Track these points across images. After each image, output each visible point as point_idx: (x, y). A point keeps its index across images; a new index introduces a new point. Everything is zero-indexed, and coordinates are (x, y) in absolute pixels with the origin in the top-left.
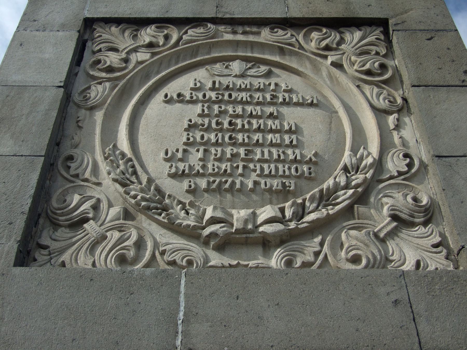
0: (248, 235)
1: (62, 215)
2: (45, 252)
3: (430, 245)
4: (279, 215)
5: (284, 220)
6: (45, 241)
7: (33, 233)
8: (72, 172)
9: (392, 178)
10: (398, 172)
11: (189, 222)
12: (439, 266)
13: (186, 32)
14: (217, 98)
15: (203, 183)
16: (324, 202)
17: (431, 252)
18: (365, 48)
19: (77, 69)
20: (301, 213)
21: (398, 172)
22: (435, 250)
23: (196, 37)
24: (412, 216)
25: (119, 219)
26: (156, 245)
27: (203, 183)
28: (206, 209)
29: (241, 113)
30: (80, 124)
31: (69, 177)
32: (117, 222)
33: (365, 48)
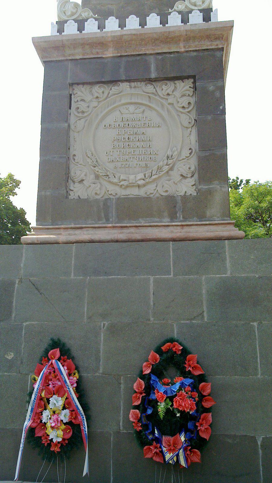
0: (133, 185)
1: (75, 178)
2: (73, 192)
3: (191, 185)
4: (143, 177)
5: (145, 178)
6: (72, 188)
7: (67, 185)
8: (76, 161)
9: (183, 159)
10: (186, 157)
11: (115, 181)
12: (192, 193)
13: (111, 89)
14: (124, 126)
15: (119, 164)
16: (159, 171)
17: (190, 188)
18: (184, 92)
19: (75, 379)
20: (150, 176)
21: (186, 157)
22: (192, 187)
23: (115, 92)
24: (187, 175)
25: (93, 179)
26: (106, 188)
27: (119, 164)
28: (120, 175)
29: (132, 134)
30: (75, 140)
31: (75, 163)
32: (93, 180)
33: (184, 92)
